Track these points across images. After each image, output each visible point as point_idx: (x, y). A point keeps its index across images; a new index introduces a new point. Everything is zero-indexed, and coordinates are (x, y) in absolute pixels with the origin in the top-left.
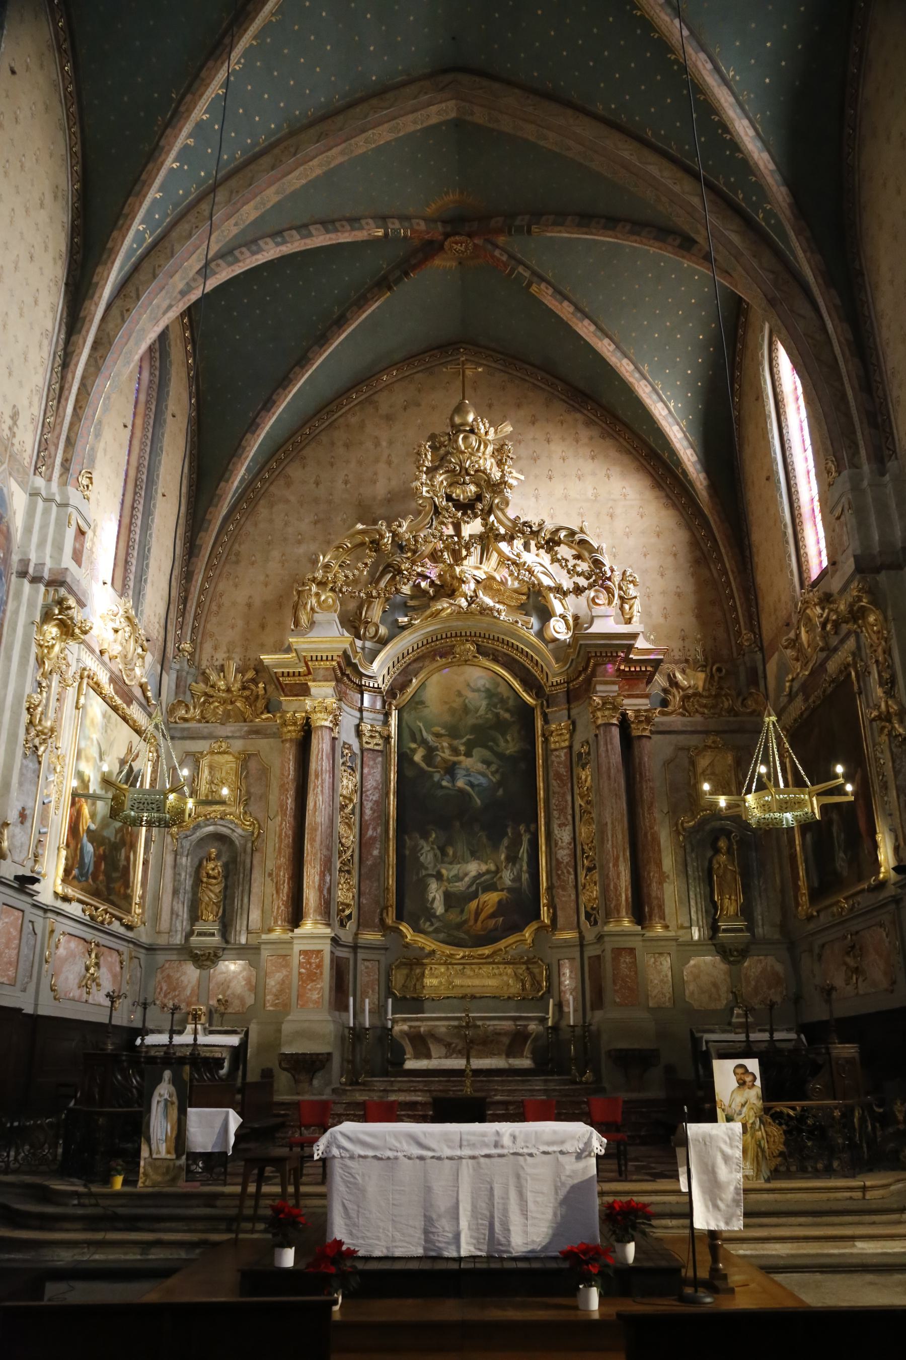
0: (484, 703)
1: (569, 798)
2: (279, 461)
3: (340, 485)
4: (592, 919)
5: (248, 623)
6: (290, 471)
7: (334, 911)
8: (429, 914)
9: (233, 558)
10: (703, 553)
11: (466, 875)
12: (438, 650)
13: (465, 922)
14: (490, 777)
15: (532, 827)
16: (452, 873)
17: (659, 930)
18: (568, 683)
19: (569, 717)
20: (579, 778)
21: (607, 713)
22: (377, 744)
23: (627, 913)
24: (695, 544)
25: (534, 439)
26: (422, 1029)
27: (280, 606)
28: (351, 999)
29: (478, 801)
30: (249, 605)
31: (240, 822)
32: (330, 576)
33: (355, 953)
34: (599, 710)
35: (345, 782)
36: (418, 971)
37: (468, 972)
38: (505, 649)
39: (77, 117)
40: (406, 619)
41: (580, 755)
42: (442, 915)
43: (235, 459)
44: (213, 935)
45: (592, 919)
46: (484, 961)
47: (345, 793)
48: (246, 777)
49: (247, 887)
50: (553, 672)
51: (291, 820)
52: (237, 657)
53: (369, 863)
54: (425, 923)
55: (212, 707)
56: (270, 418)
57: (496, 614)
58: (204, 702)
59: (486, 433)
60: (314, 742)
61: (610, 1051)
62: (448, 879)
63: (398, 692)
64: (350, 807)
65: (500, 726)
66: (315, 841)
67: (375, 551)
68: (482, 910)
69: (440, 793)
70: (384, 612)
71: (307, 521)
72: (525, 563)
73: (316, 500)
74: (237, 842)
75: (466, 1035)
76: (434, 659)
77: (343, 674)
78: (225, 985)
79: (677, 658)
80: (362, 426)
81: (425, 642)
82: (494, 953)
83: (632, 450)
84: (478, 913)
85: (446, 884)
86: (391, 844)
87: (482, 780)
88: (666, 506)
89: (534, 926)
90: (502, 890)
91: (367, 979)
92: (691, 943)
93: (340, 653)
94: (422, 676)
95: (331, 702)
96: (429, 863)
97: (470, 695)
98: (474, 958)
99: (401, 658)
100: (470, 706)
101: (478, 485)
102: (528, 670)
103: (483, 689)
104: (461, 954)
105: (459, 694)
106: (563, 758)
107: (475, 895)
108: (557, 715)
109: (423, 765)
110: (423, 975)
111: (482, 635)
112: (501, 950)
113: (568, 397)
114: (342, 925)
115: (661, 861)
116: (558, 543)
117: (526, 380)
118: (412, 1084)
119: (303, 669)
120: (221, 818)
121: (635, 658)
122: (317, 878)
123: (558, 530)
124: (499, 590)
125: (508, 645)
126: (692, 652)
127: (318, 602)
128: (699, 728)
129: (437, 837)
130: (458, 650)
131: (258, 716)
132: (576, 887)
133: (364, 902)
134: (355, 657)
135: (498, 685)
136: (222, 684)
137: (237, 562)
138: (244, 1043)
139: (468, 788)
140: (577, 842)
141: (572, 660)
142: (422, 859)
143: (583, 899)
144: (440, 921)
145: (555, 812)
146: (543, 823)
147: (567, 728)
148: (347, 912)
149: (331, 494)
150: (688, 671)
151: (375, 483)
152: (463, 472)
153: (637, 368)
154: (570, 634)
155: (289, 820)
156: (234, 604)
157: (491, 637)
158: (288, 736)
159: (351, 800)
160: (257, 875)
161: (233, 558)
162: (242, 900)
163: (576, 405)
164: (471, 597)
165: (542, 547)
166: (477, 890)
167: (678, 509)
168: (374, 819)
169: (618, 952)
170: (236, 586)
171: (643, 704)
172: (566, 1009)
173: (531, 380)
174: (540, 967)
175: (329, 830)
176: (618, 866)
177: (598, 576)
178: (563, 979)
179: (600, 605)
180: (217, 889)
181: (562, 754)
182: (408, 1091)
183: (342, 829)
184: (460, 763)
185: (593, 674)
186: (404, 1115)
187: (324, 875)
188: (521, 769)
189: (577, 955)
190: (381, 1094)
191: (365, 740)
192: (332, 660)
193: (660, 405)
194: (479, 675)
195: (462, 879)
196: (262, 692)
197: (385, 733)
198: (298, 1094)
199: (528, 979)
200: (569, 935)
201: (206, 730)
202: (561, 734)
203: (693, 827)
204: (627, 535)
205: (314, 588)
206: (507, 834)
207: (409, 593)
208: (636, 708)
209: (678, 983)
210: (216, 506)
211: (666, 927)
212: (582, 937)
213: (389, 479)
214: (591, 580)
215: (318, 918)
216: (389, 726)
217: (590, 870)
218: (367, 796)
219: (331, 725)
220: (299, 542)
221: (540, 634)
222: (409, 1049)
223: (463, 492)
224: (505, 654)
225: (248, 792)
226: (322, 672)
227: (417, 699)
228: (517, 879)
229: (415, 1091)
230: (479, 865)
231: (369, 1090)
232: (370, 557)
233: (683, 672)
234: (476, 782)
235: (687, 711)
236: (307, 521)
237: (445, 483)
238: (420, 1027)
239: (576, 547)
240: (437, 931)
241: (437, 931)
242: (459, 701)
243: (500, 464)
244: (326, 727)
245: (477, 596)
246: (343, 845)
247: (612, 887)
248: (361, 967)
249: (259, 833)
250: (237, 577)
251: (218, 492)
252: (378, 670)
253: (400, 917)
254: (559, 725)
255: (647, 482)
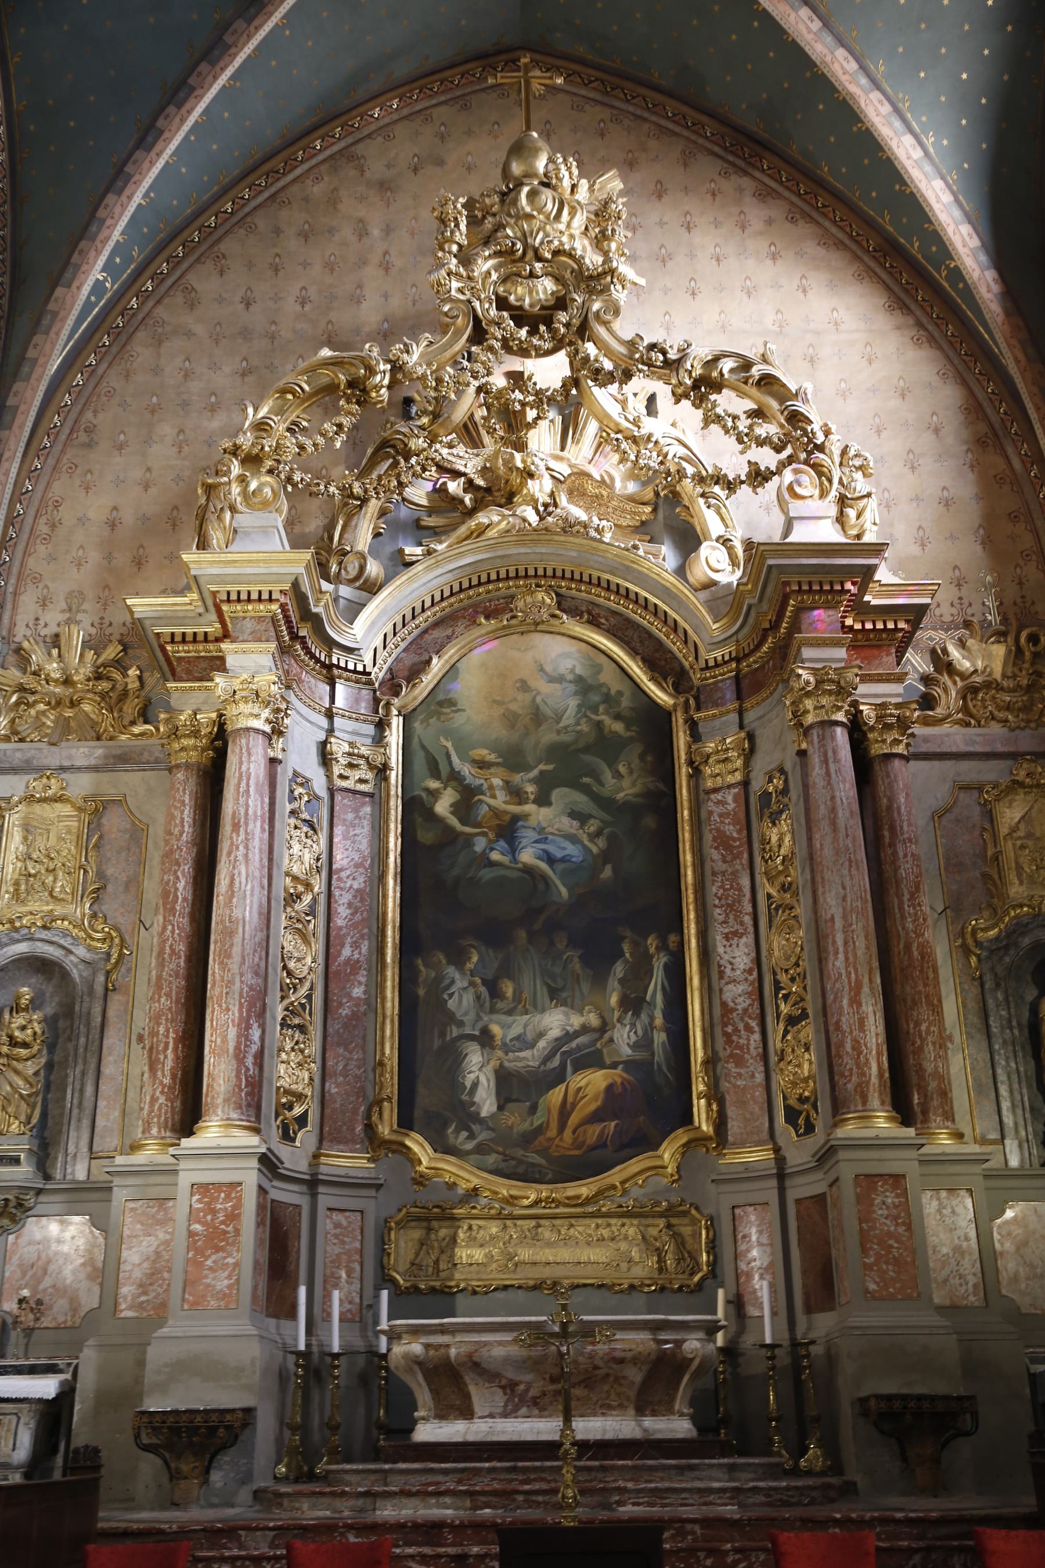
0: (573, 703)
1: (745, 882)
2: (175, 262)
3: (291, 306)
4: (801, 1121)
5: (109, 557)
6: (192, 279)
7: (268, 1107)
8: (468, 1117)
9: (83, 437)
10: (991, 426)
11: (541, 1035)
12: (480, 603)
13: (540, 1130)
14: (586, 842)
15: (673, 938)
16: (516, 1030)
17: (944, 1142)
18: (738, 660)
19: (741, 727)
20: (765, 841)
21: (824, 701)
22: (361, 781)
23: (883, 1103)
24: (973, 410)
25: (661, 224)
26: (453, 1352)
27: (174, 525)
28: (302, 1291)
29: (564, 891)
30: (113, 525)
31: (82, 934)
32: (268, 444)
33: (314, 1195)
34: (808, 694)
35: (296, 848)
36: (443, 1232)
37: (546, 1233)
38: (612, 602)
39: (8, 193)
40: (419, 550)
41: (766, 796)
42: (492, 1116)
43: (83, 244)
44: (16, 1161)
45: (801, 1121)
46: (579, 1210)
47: (296, 869)
48: (97, 846)
49: (93, 1066)
50: (710, 636)
51: (185, 921)
52: (86, 620)
53: (345, 1012)
54: (457, 1131)
55: (33, 712)
56: (152, 163)
57: (593, 533)
58: (17, 704)
59: (574, 187)
60: (232, 760)
61: (863, 1401)
62: (504, 1044)
63: (404, 683)
64: (307, 899)
65: (605, 746)
66: (229, 956)
67: (358, 403)
68: (574, 1105)
69: (487, 874)
70: (377, 535)
71: (227, 369)
72: (650, 436)
73: (245, 333)
74: (75, 974)
75: (561, 1355)
76: (474, 623)
77: (294, 636)
78: (39, 1268)
79: (947, 618)
80: (333, 201)
81: (456, 588)
82: (600, 1193)
83: (847, 242)
84: (565, 1111)
85: (500, 1053)
86: (389, 973)
87: (571, 850)
88: (917, 342)
89: (681, 1137)
90: (614, 1066)
91: (337, 1250)
92: (1006, 1174)
93: (287, 587)
94: (451, 652)
95: (268, 680)
96: (466, 1014)
97: (544, 688)
98: (559, 1203)
99: (409, 617)
100: (544, 709)
101: (558, 279)
102: (660, 643)
103: (570, 677)
104: (533, 1197)
105: (524, 686)
106: (731, 806)
107: (559, 1077)
108: (717, 723)
109: (454, 822)
110: (454, 1240)
111: (568, 575)
112: (613, 1187)
113: (725, 149)
114: (287, 1136)
115: (940, 1001)
116: (717, 386)
117: (645, 120)
118: (431, 1478)
119: (214, 628)
120: (45, 927)
121: (875, 602)
122: (232, 1033)
123: (716, 359)
124: (598, 497)
125: (618, 593)
126: (976, 608)
127: (244, 493)
128: (1000, 748)
129: (481, 959)
130: (520, 604)
131: (124, 728)
132: (765, 1057)
133: (334, 1090)
134: (318, 601)
135: (598, 669)
136: (53, 668)
137: (89, 445)
138: (67, 1393)
139: (543, 866)
140: (765, 968)
141: (750, 607)
142: (451, 1004)
143: (779, 1081)
144: (489, 1128)
145: (718, 911)
146: (693, 931)
147: (738, 746)
148: (298, 1110)
149: (274, 322)
150: (970, 642)
151: (359, 302)
152: (530, 254)
153: (863, 68)
154: (739, 573)
155: (182, 920)
156: (82, 521)
157: (586, 578)
158: (182, 759)
159: (308, 886)
160: (112, 1040)
161: (83, 437)
162: (82, 1091)
163: (740, 162)
164: (546, 506)
165: (686, 396)
166: (563, 1066)
167: (940, 348)
168: (355, 926)
169: (869, 1181)
170: (87, 489)
171: (891, 692)
172: (752, 1311)
173: (654, 118)
174: (695, 1222)
175: (261, 936)
176: (860, 1005)
177: (799, 441)
178: (742, 1247)
179: (803, 498)
180: (30, 1068)
181: (730, 799)
182: (423, 1494)
183: (289, 942)
184: (525, 816)
185: (795, 626)
186: (412, 1557)
187: (248, 1027)
188: (650, 825)
189: (773, 1197)
190: (360, 1502)
191: (337, 770)
192: (270, 600)
193: (908, 140)
194: (561, 653)
195: (532, 1045)
196: (133, 685)
197: (379, 760)
198: (175, 1505)
199: (669, 1247)
200: (757, 1156)
201: (19, 755)
202: (726, 760)
203: (997, 939)
204: (844, 395)
205: (236, 469)
206: (622, 954)
207: (424, 502)
208: (879, 701)
209: (988, 1257)
210: (47, 333)
211: (959, 1136)
212: (780, 1161)
213: (386, 296)
214: (785, 454)
215: (234, 1115)
216: (386, 746)
217: (792, 1021)
218: (339, 879)
219: (267, 728)
220: (213, 409)
221: (681, 572)
222: (423, 1396)
223: (530, 292)
224: (615, 613)
225: (100, 875)
226: (249, 625)
227: (441, 697)
228: (644, 1043)
229: (438, 1494)
230: (567, 1015)
231: (333, 1494)
232: (349, 413)
233: (962, 644)
234: (559, 854)
235: (972, 716)
236: (227, 369)
237: (494, 276)
238: (448, 1346)
239: (754, 391)
240: (481, 1149)
241: (481, 1149)
242: (524, 698)
243: (600, 241)
244: (257, 731)
245: (556, 505)
246: (290, 974)
247: (848, 1046)
248: (326, 1224)
249: (121, 955)
250: (90, 471)
251: (51, 306)
252: (365, 635)
253: (406, 1122)
254: (722, 738)
255: (880, 300)
